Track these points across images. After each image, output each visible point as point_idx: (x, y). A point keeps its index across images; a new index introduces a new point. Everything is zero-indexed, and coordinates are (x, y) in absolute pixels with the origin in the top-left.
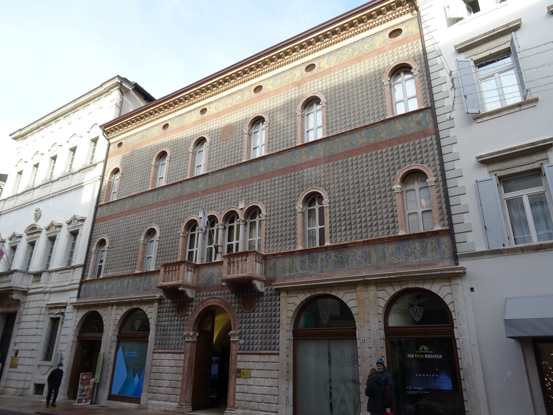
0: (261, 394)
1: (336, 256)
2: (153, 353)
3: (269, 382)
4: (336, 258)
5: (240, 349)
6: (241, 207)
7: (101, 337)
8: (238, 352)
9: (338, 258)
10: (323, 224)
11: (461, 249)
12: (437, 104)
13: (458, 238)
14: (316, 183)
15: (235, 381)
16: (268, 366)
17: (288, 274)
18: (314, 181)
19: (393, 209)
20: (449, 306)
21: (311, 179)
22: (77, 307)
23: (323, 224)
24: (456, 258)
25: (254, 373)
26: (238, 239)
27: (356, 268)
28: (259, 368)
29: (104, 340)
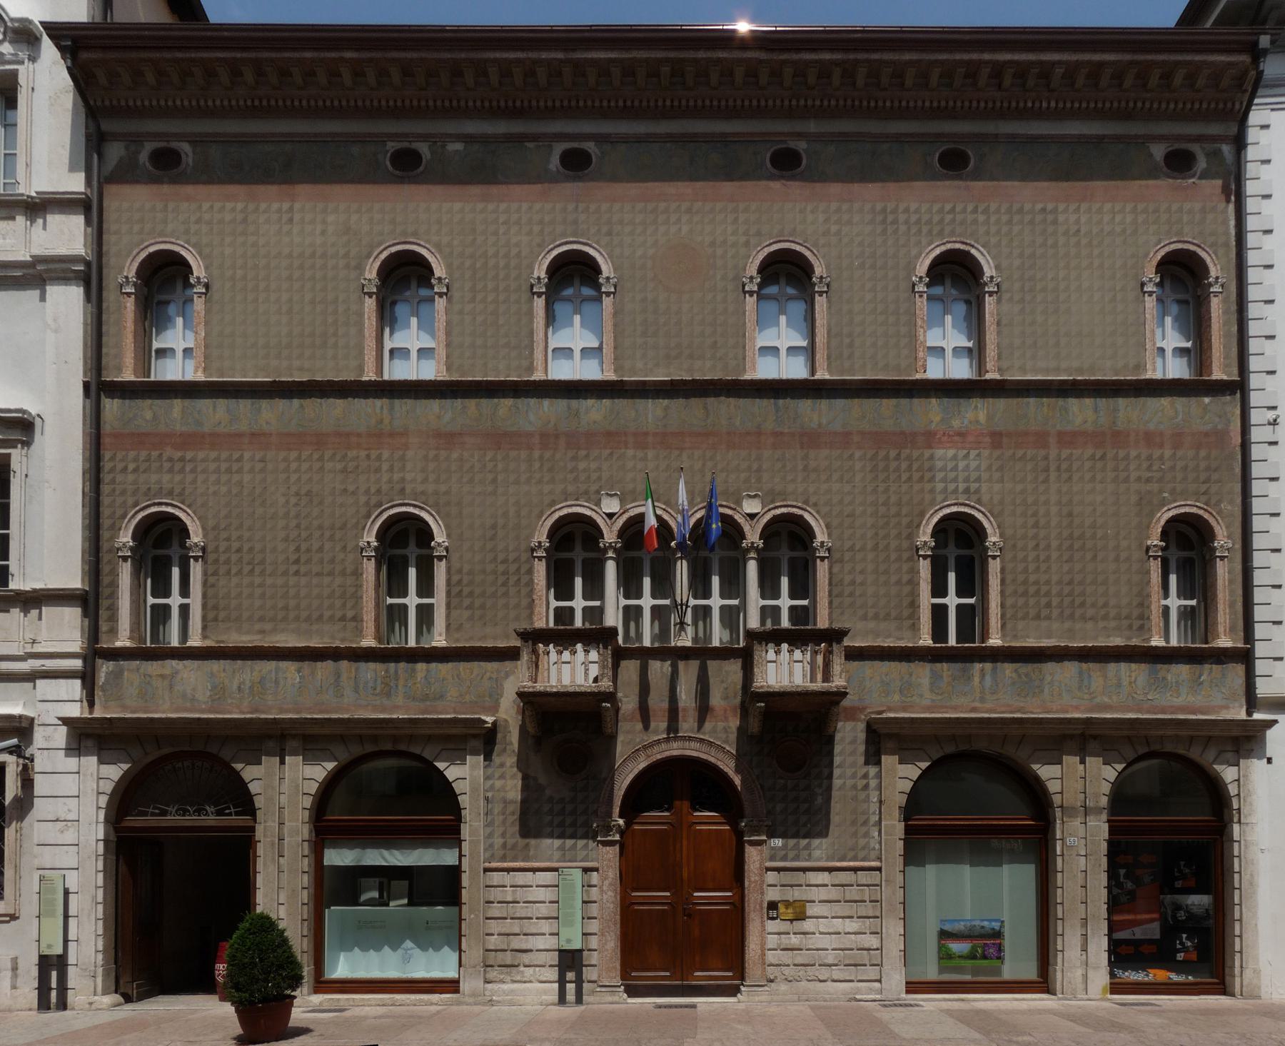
0: (855, 933)
1: (1016, 671)
2: (486, 870)
3: (852, 926)
4: (1014, 675)
5: (772, 859)
6: (752, 511)
7: (253, 829)
8: (769, 864)
9: (1019, 676)
10: (430, 594)
11: (1263, 688)
12: (1254, 381)
13: (1260, 667)
14: (967, 491)
15: (763, 926)
16: (853, 893)
17: (897, 697)
18: (962, 487)
19: (114, 523)
20: (1230, 787)
21: (955, 480)
22: (87, 737)
23: (430, 594)
24: (1252, 703)
25: (811, 910)
26: (185, 592)
27: (1065, 695)
28: (831, 897)
29: (259, 833)
